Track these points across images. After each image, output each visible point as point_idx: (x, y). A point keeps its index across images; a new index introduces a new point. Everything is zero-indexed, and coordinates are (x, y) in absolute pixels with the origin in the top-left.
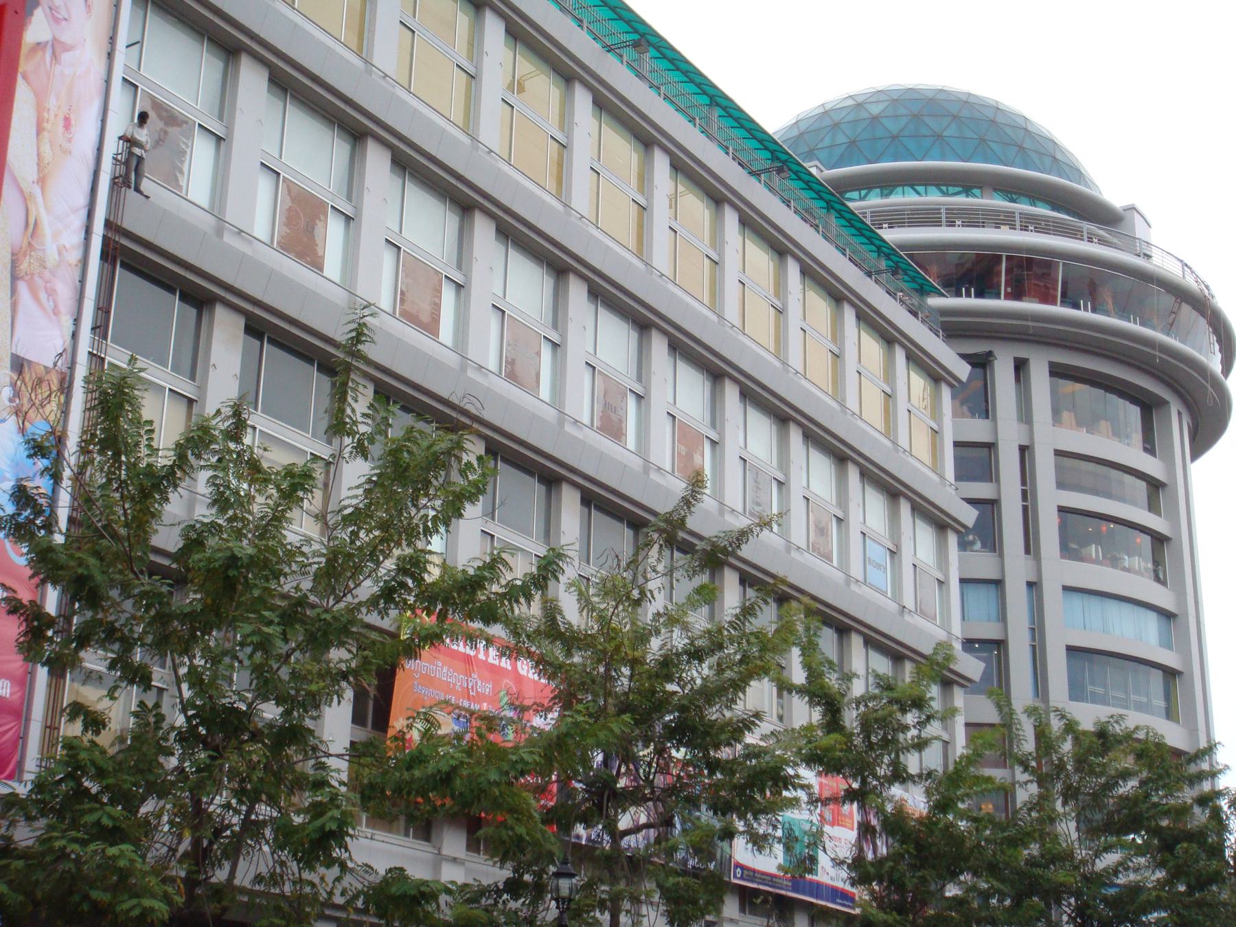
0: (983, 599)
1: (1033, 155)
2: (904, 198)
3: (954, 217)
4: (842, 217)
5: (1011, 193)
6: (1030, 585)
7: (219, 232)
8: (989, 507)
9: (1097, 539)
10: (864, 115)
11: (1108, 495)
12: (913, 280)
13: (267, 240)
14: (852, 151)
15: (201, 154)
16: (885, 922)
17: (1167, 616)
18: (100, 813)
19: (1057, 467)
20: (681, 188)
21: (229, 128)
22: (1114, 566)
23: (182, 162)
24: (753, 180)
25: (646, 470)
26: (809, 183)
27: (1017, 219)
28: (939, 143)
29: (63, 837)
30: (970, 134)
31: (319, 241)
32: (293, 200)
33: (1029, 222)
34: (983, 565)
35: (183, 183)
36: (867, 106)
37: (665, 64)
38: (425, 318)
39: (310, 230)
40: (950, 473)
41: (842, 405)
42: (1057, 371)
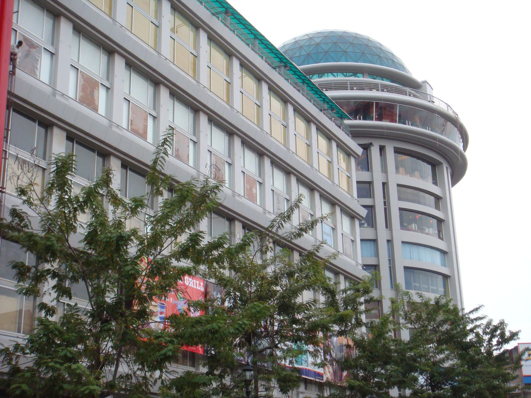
0: (370, 246)
1: (384, 60)
2: (329, 78)
3: (353, 86)
4: (309, 86)
5: (373, 75)
6: (388, 241)
7: (54, 95)
8: (371, 208)
9: (415, 221)
10: (313, 43)
11: (419, 203)
12: (338, 113)
13: (74, 98)
14: (308, 58)
15: (45, 61)
16: (359, 385)
17: (444, 253)
18: (65, 351)
19: (398, 191)
20: (244, 74)
21: (57, 49)
22: (422, 233)
23: (37, 64)
24: (274, 70)
25: (234, 196)
26: (296, 72)
27: (380, 87)
28: (345, 54)
29: (51, 361)
30: (358, 51)
31: (96, 98)
32: (84, 81)
33: (384, 88)
34: (369, 234)
35: (38, 73)
36: (314, 39)
37: (236, 21)
38: (141, 131)
39: (92, 94)
40: (355, 195)
41: (312, 166)
42: (397, 151)
